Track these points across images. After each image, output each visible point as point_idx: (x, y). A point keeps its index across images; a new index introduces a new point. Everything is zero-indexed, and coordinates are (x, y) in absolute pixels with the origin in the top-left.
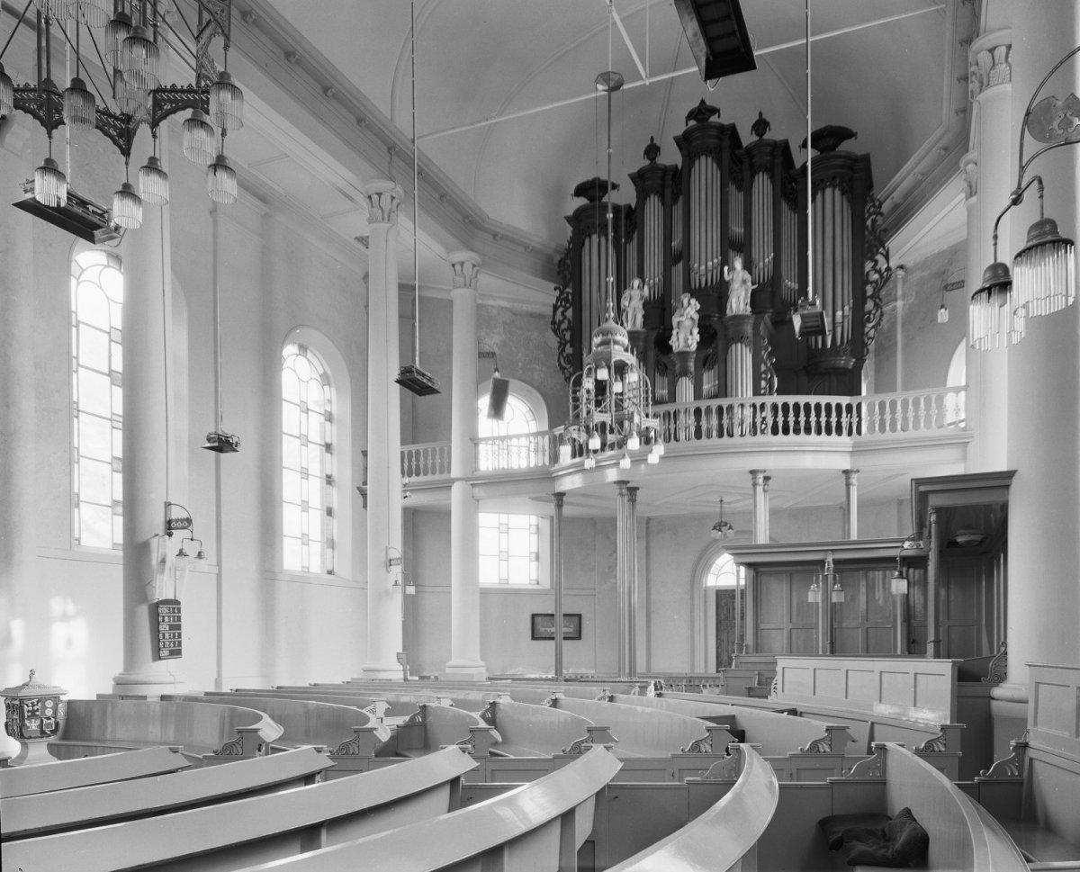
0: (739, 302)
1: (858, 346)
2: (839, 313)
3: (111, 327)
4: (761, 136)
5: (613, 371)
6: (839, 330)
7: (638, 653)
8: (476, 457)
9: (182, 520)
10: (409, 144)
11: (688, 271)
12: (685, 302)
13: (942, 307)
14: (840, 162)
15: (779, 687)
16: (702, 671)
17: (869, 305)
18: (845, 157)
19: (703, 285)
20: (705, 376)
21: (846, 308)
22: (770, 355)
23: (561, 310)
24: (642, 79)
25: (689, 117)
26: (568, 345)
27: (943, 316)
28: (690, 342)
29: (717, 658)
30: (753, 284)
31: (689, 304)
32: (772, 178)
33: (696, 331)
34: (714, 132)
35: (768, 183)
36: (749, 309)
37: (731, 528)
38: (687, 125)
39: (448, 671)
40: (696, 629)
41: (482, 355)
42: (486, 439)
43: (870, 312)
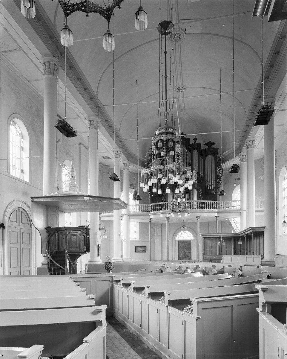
1: (217, 188)
2: (213, 182)
3: (15, 170)
4: (195, 141)
6: (212, 185)
7: (200, 255)
9: (103, 228)
10: (124, 140)
13: (235, 183)
14: (212, 149)
15: (223, 260)
16: (175, 260)
17: (218, 180)
18: (213, 149)
20: (187, 195)
22: (201, 191)
29: (179, 256)
32: (198, 151)
34: (185, 140)
35: (197, 152)
39: (112, 260)
40: (174, 248)
41: (130, 185)
42: (131, 205)
43: (219, 182)
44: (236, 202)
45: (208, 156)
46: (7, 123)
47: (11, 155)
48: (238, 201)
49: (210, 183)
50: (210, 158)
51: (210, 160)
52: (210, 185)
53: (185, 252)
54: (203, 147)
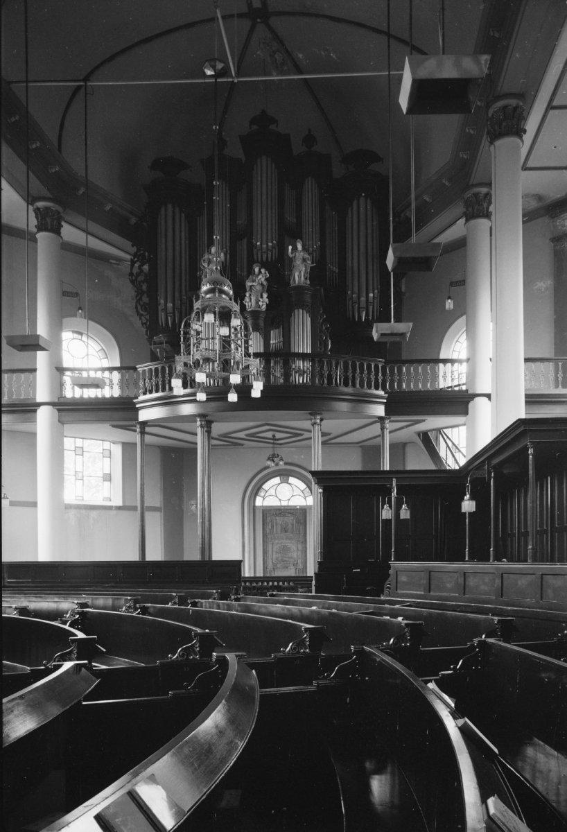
0: (299, 275)
2: (371, 295)
5: (217, 316)
8: (61, 385)
11: (251, 246)
12: (257, 270)
13: (449, 298)
19: (269, 260)
21: (376, 291)
23: (136, 265)
24: (231, 76)
25: (253, 122)
26: (145, 295)
27: (449, 304)
28: (260, 303)
30: (312, 263)
31: (260, 272)
33: (265, 295)
36: (308, 282)
37: (281, 459)
38: (250, 128)
41: (65, 293)
44: (453, 365)
45: (259, 160)
46: (449, 365)
47: (63, 351)
48: (460, 361)
49: (363, 299)
50: (361, 209)
51: (362, 217)
52: (363, 304)
53: (285, 549)
54: (338, 171)
